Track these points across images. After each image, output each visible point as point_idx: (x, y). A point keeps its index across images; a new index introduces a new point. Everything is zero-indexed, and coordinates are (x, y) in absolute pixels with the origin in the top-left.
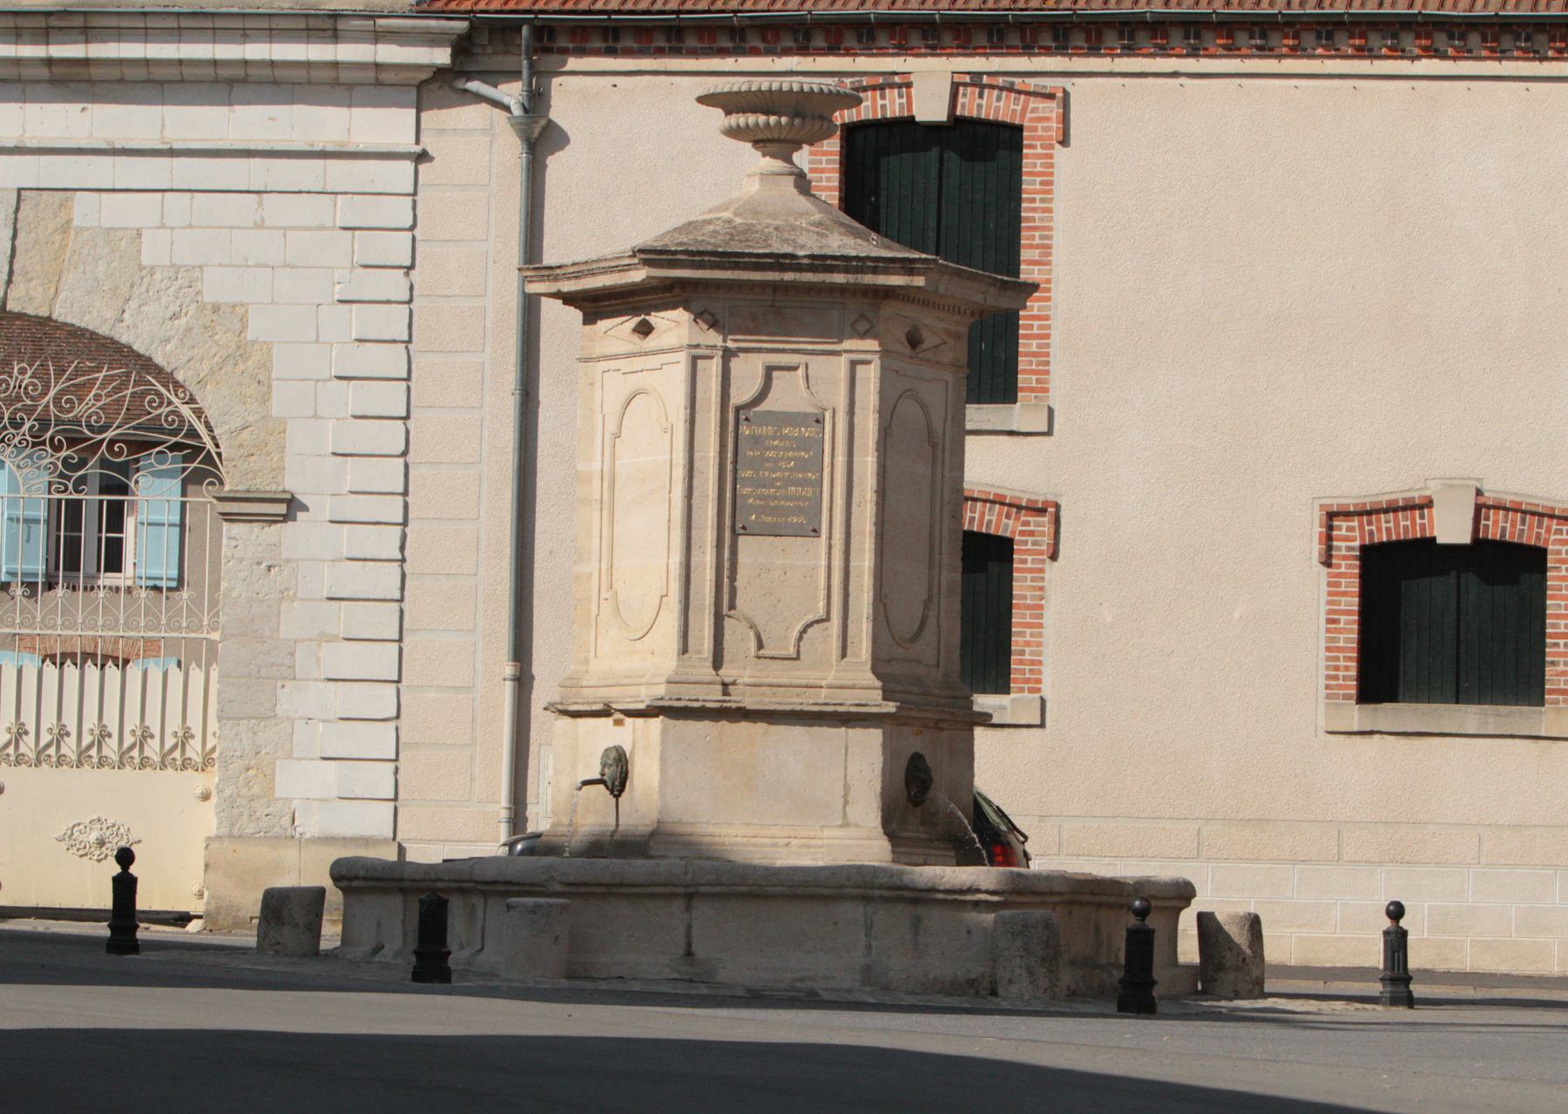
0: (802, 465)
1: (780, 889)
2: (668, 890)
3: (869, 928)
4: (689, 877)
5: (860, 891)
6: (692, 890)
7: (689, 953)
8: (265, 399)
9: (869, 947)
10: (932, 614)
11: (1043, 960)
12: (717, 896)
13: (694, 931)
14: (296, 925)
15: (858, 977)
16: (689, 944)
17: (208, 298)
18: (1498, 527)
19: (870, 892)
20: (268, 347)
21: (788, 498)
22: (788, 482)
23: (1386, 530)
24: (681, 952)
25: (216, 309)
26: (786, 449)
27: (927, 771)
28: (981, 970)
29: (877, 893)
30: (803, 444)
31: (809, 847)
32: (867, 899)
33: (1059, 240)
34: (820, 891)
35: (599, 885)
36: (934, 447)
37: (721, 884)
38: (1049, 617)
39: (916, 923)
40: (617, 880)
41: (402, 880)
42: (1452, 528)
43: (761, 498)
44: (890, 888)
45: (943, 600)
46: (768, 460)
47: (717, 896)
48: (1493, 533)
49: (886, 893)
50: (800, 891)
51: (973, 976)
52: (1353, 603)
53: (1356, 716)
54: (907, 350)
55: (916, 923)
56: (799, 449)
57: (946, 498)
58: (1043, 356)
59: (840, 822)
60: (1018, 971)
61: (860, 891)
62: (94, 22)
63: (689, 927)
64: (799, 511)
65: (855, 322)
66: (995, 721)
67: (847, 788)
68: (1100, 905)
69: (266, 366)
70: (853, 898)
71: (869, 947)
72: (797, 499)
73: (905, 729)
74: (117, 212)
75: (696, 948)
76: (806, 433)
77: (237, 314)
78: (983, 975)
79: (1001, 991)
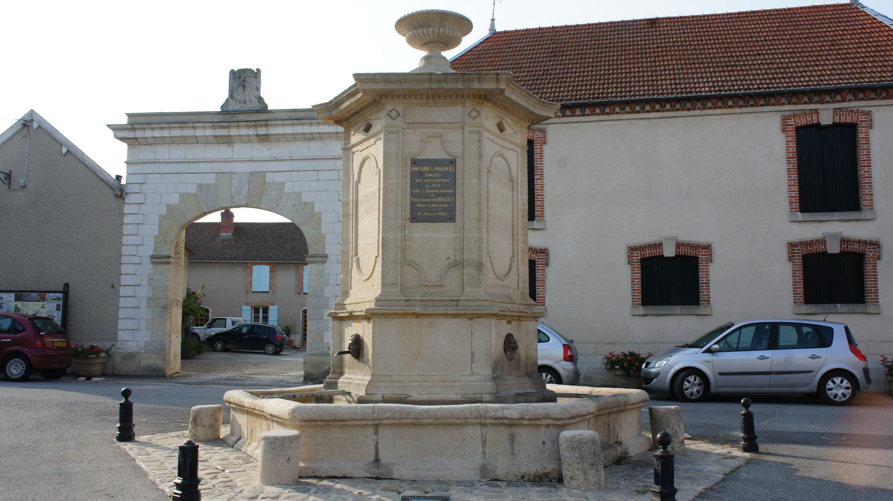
0: (445, 186)
1: (430, 421)
2: (363, 423)
3: (484, 442)
4: (375, 415)
5: (478, 421)
6: (377, 422)
7: (377, 460)
8: (320, 228)
9: (484, 453)
10: (515, 265)
11: (592, 464)
12: (393, 425)
13: (380, 446)
14: (204, 426)
15: (478, 473)
16: (377, 453)
17: (303, 201)
18: (684, 251)
19: (483, 421)
20: (320, 214)
21: (438, 203)
22: (437, 195)
23: (648, 253)
24: (373, 458)
25: (306, 204)
26: (436, 178)
27: (515, 342)
28: (551, 467)
29: (488, 421)
30: (445, 175)
31: (453, 387)
32: (483, 425)
33: (545, 172)
34: (454, 421)
35: (322, 420)
36: (512, 181)
37: (395, 419)
38: (547, 284)
39: (512, 438)
40: (332, 418)
41: (243, 406)
42: (669, 252)
43: (426, 203)
44: (496, 419)
45: (520, 257)
46: (427, 183)
47: (393, 425)
48: (682, 253)
49: (493, 421)
50: (442, 421)
51: (547, 471)
52: (639, 276)
53: (641, 310)
54: (497, 131)
55: (512, 438)
56: (442, 177)
57: (520, 208)
58: (542, 206)
59: (469, 373)
60: (576, 472)
61: (478, 421)
62: (269, 123)
63: (377, 444)
64: (444, 209)
65: (471, 112)
66: (13, 295)
67: (473, 355)
68: (609, 414)
69: (320, 219)
70: (474, 424)
71: (484, 453)
72: (443, 203)
73: (502, 321)
74: (278, 178)
75: (381, 456)
76: (446, 169)
77: (312, 204)
78: (553, 470)
79: (565, 482)
